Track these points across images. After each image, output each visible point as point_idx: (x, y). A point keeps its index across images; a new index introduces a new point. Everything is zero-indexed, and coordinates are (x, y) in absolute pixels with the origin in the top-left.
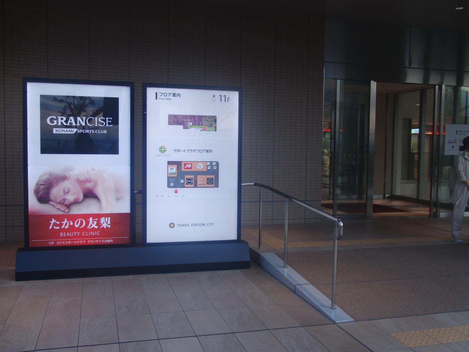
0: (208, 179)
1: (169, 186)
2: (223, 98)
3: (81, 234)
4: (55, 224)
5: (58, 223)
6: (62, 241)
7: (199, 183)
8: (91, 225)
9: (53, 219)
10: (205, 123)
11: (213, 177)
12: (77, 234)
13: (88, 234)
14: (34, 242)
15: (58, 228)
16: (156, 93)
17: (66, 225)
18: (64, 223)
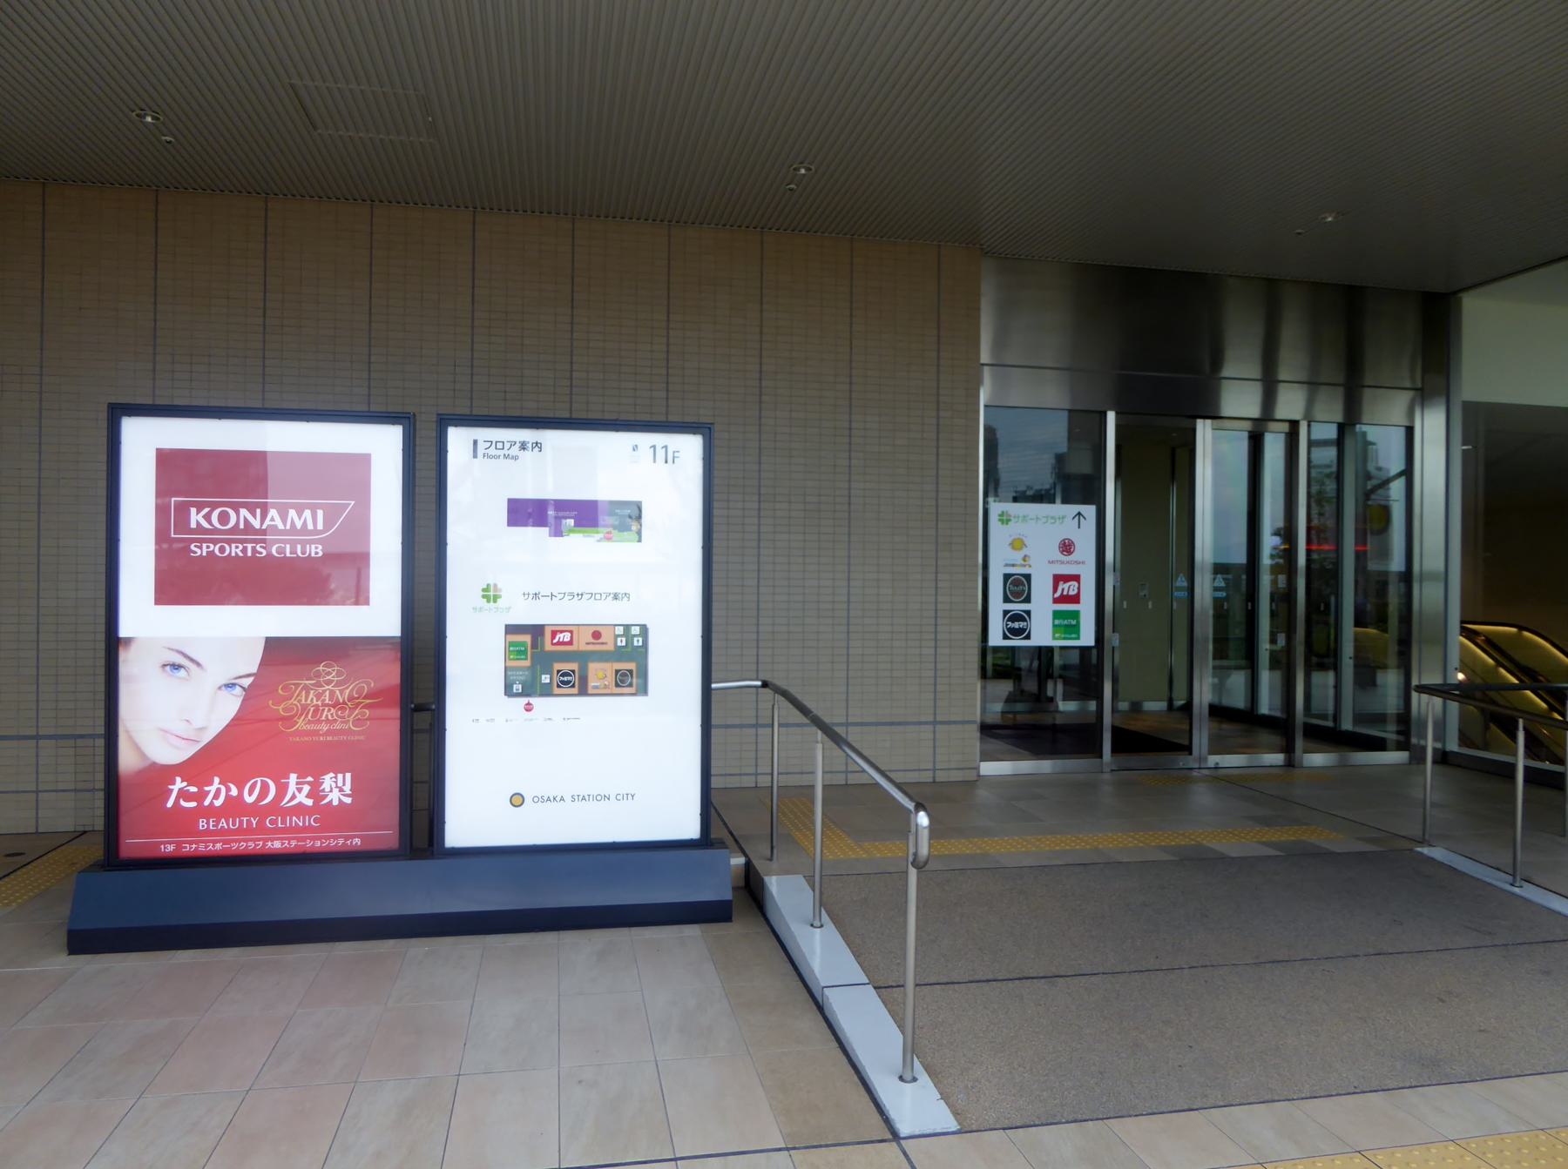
0: (617, 672)
1: (509, 692)
2: (661, 453)
3: (261, 823)
4: (183, 794)
5: (193, 789)
6: (197, 842)
7: (591, 684)
8: (294, 797)
9: (178, 779)
10: (611, 520)
11: (632, 666)
12: (249, 822)
13: (284, 822)
14: (133, 843)
15: (193, 804)
16: (475, 442)
17: (216, 796)
18: (212, 789)
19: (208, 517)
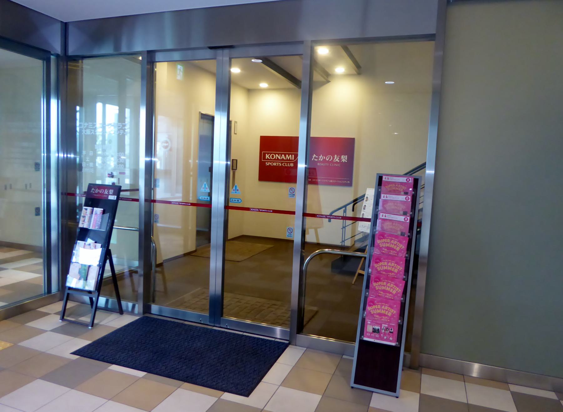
4: (315, 158)
19: (269, 156)
